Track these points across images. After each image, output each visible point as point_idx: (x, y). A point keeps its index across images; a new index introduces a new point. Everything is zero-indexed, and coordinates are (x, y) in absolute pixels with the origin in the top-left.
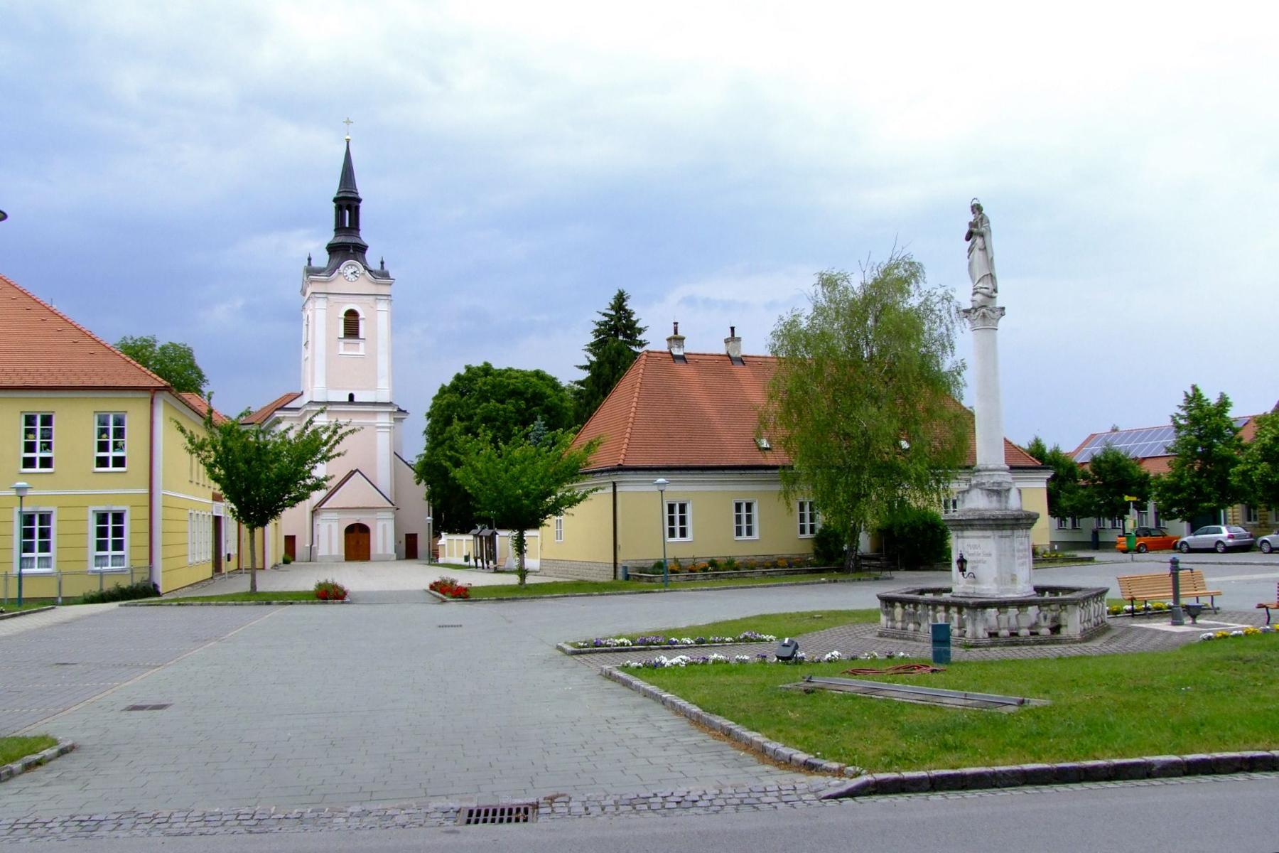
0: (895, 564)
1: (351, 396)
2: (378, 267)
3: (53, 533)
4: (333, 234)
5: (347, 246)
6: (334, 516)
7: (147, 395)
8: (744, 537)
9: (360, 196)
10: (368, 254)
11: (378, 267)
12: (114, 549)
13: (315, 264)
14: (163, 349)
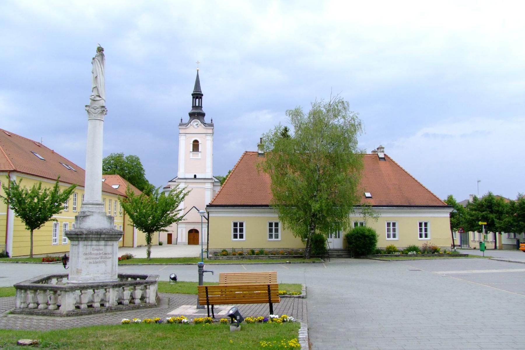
0: (350, 255)
1: (195, 176)
2: (210, 122)
3: (397, 230)
4: (191, 108)
5: (197, 114)
6: (184, 225)
7: (7, 174)
8: (274, 239)
9: (203, 93)
10: (205, 118)
11: (210, 122)
12: (240, 238)
13: (184, 122)
14: (127, 158)
